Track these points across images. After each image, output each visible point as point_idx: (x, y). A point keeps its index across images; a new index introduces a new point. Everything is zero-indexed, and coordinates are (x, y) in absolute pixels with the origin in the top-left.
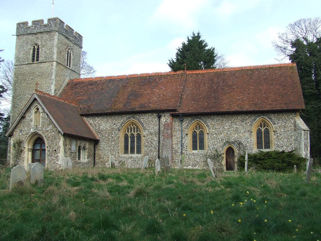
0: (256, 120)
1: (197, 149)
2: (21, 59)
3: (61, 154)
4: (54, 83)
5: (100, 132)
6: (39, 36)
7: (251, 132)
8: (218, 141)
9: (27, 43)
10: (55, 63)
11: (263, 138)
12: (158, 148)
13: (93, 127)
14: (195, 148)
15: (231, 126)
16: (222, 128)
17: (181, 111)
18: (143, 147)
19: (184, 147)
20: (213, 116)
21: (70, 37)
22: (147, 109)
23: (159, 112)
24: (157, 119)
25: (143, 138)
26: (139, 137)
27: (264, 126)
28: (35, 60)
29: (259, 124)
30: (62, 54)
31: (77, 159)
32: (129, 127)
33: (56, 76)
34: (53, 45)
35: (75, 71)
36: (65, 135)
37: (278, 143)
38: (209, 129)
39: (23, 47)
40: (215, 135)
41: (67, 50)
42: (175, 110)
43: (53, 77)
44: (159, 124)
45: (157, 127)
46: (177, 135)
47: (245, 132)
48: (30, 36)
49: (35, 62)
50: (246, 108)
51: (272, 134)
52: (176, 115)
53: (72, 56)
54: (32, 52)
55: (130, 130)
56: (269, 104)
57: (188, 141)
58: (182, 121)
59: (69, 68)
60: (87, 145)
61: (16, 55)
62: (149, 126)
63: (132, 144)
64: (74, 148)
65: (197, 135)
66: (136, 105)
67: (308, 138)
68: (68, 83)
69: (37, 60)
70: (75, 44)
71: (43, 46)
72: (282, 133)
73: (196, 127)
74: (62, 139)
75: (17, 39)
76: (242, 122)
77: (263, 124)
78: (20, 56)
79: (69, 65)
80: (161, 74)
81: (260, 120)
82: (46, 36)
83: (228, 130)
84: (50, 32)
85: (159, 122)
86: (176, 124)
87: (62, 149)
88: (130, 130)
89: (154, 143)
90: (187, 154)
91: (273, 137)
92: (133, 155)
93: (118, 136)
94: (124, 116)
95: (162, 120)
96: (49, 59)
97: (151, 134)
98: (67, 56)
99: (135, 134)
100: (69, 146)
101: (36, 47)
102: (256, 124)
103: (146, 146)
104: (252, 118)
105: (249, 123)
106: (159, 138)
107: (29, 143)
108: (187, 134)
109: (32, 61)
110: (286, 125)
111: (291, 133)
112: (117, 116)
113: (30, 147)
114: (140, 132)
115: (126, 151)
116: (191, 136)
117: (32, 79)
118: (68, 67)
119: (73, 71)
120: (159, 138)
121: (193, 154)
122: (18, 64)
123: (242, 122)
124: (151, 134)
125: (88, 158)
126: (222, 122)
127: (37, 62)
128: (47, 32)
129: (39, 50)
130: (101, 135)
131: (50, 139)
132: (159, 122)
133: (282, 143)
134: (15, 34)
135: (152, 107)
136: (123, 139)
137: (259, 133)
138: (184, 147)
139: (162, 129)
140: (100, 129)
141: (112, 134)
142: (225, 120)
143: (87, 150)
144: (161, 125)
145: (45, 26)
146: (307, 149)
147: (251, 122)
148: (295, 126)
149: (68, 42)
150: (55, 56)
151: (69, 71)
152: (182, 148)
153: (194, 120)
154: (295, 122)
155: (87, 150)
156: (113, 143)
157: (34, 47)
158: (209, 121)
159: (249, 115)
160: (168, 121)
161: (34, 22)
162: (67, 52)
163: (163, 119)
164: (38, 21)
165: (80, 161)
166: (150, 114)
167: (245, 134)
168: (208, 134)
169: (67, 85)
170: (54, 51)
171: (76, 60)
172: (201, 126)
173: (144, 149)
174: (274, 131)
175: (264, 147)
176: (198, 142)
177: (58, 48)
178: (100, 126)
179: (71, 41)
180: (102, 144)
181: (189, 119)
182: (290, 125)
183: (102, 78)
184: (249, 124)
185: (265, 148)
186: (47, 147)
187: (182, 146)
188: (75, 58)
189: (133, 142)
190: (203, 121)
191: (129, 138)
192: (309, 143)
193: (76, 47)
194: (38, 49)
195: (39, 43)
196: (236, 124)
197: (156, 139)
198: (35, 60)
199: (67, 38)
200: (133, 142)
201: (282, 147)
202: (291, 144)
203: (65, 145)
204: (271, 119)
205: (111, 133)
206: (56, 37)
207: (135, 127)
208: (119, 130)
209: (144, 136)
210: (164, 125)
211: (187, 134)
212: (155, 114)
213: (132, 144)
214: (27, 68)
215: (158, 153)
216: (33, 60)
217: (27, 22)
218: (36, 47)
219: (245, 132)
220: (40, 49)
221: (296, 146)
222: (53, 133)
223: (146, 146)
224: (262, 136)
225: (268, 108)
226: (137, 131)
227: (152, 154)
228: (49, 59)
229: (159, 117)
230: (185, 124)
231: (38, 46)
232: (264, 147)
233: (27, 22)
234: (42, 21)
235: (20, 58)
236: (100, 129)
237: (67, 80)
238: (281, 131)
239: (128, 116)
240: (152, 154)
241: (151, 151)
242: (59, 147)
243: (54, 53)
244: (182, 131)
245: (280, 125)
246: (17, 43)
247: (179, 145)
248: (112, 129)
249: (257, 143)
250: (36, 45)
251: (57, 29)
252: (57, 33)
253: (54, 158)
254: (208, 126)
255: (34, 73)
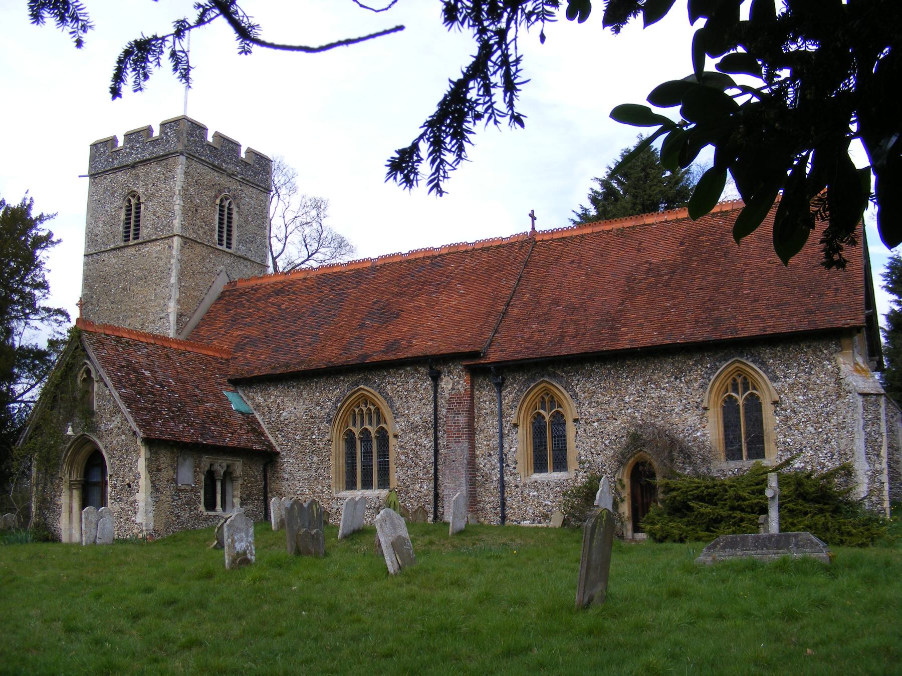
0: (718, 369)
1: (547, 465)
2: (98, 238)
3: (142, 497)
4: (175, 294)
5: (279, 427)
6: (141, 171)
7: (705, 409)
8: (607, 442)
9: (113, 194)
10: (176, 241)
11: (744, 429)
12: (432, 471)
13: (263, 414)
14: (540, 465)
15: (642, 395)
16: (618, 400)
17: (494, 356)
18: (392, 466)
19: (507, 465)
20: (588, 367)
21: (227, 164)
22: (402, 355)
23: (434, 365)
24: (429, 383)
25: (392, 442)
26: (383, 437)
27: (746, 389)
28: (132, 236)
29: (730, 381)
30: (202, 213)
31: (202, 508)
32: (357, 410)
33: (182, 275)
34: (171, 195)
35: (249, 255)
36: (149, 442)
37: (789, 440)
38: (580, 404)
39: (103, 205)
40: (595, 424)
41: (218, 201)
42: (475, 355)
43: (173, 280)
44: (435, 397)
45: (430, 408)
46: (488, 426)
47: (686, 409)
48: (119, 174)
49: (131, 243)
50: (688, 333)
51: (768, 410)
52: (483, 370)
53: (235, 216)
54: (123, 216)
55: (358, 418)
56: (757, 317)
57: (519, 445)
58: (500, 386)
59: (228, 250)
60: (239, 467)
61: (88, 227)
62: (407, 407)
63: (367, 460)
64: (187, 474)
65: (545, 426)
66: (375, 348)
67: (879, 419)
68: (223, 293)
69: (137, 236)
70: (245, 182)
71: (150, 197)
72: (800, 407)
73: (543, 402)
74: (143, 452)
75: (92, 184)
76: (676, 378)
77: (739, 380)
78: (96, 231)
79: (225, 243)
80: (464, 249)
81: (730, 369)
82: (156, 169)
83: (635, 407)
84: (166, 156)
85: (436, 392)
86: (486, 399)
87: (144, 482)
88: (358, 418)
89: (424, 454)
90: (517, 486)
91: (771, 419)
92: (368, 493)
93: (327, 437)
94: (342, 378)
95: (443, 384)
96: (162, 230)
97: (414, 428)
98: (217, 217)
99: (373, 430)
100: (171, 473)
101: (133, 201)
102: (717, 384)
103: (402, 465)
104: (707, 363)
105: (696, 380)
106: (436, 439)
107: (71, 465)
108: (516, 426)
109: (125, 241)
110: (809, 379)
111: (826, 406)
112: (324, 379)
113: (74, 478)
114: (385, 423)
115: (351, 485)
116: (530, 429)
117: (124, 289)
118: (224, 248)
119: (239, 257)
120: (436, 439)
121: (535, 485)
122: (94, 251)
123: (676, 378)
124: (414, 428)
125: (242, 505)
126: (616, 383)
127: (136, 242)
128: (159, 159)
129: (140, 208)
130: (283, 436)
131: (117, 454)
132: (436, 392)
133: (799, 437)
134: (87, 173)
135: (422, 346)
136: (342, 445)
137: (729, 407)
138: (507, 465)
139: (443, 411)
140: (282, 419)
141: (313, 433)
142: (625, 375)
143: (240, 482)
144: (442, 402)
145: (156, 142)
146: (878, 455)
147: (703, 378)
148: (838, 381)
149: (223, 180)
150: (177, 222)
151: (228, 260)
152: (502, 467)
153: (534, 380)
154: (839, 369)
155: (240, 482)
156: (315, 459)
157: (129, 201)
158: (578, 380)
159: (697, 357)
160: (460, 386)
161: (128, 136)
162: (218, 207)
163: (446, 384)
164: (137, 133)
165: (210, 513)
166: (409, 369)
167: (685, 415)
168: (576, 420)
169: (219, 299)
170: (177, 207)
171: (252, 227)
172: (749, 380)
173: (396, 474)
174: (775, 403)
175: (745, 453)
176: (548, 449)
177: (186, 196)
178: (290, 416)
179: (229, 175)
180: (288, 464)
181: (520, 378)
182: (821, 377)
183: (369, 260)
184: (696, 385)
185: (750, 457)
186: (111, 476)
187: (501, 460)
188: (246, 221)
189: (367, 454)
190: (561, 382)
191: (358, 443)
192: (885, 434)
193: (249, 191)
194: (138, 207)
195: (141, 191)
196: (658, 386)
197: (428, 443)
198: (132, 236)
199: (217, 168)
200: (367, 454)
201: (801, 450)
202: (827, 441)
203: (153, 469)
204: (763, 364)
205: (309, 429)
206: (180, 170)
207: (372, 408)
208: (329, 422)
209: (396, 436)
210: (449, 401)
211: (516, 426)
212: (422, 370)
213: (367, 460)
214: (112, 259)
215: (432, 485)
216: (127, 238)
217: (115, 137)
218: (133, 201)
219: (686, 409)
220: (142, 206)
221: (842, 447)
222: (123, 437)
223: (402, 465)
224: (739, 418)
225: (751, 329)
226: (378, 422)
227: (417, 487)
228: (162, 230)
229: (436, 378)
230: (509, 395)
231: (139, 198)
232: (745, 453)
233: (115, 137)
234: (149, 130)
235: (97, 236)
236: (282, 419)
237: (220, 284)
238: (795, 401)
239: (352, 379)
240: (417, 487)
241: (415, 479)
242: (137, 476)
243: (174, 214)
244: (501, 415)
245: (790, 381)
246: (91, 195)
247: (495, 459)
248: (312, 417)
249: (726, 443)
250: (134, 196)
251: (180, 148)
252: (182, 159)
253: (127, 507)
254: (575, 396)
255: (128, 271)
